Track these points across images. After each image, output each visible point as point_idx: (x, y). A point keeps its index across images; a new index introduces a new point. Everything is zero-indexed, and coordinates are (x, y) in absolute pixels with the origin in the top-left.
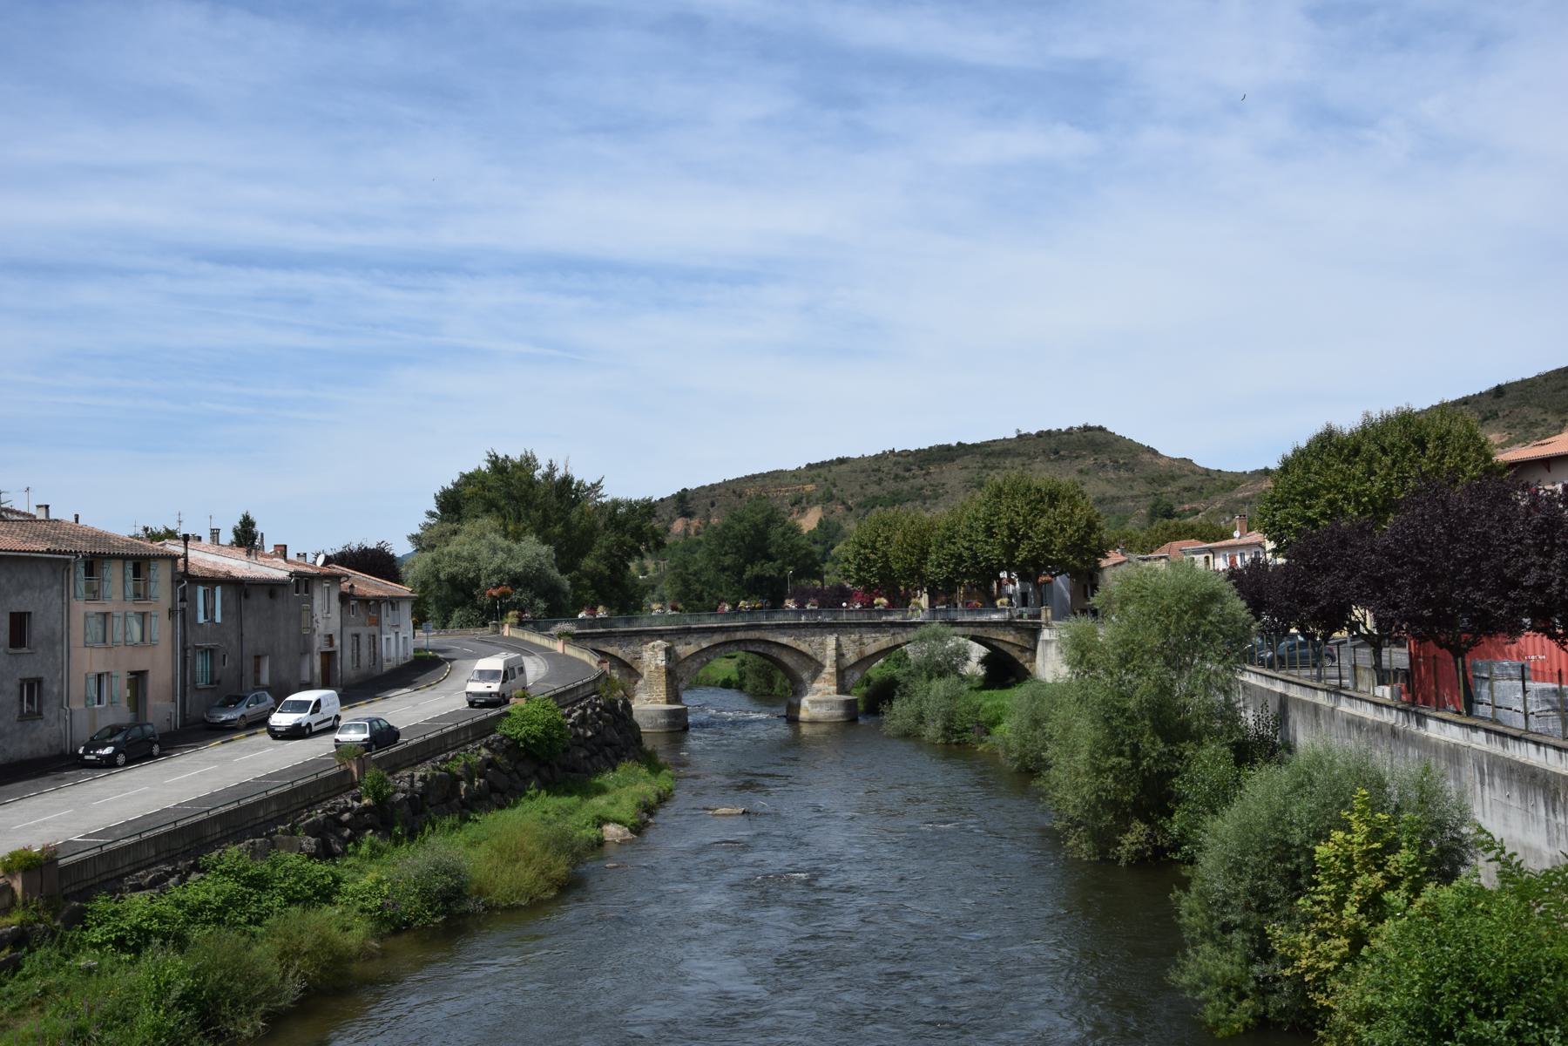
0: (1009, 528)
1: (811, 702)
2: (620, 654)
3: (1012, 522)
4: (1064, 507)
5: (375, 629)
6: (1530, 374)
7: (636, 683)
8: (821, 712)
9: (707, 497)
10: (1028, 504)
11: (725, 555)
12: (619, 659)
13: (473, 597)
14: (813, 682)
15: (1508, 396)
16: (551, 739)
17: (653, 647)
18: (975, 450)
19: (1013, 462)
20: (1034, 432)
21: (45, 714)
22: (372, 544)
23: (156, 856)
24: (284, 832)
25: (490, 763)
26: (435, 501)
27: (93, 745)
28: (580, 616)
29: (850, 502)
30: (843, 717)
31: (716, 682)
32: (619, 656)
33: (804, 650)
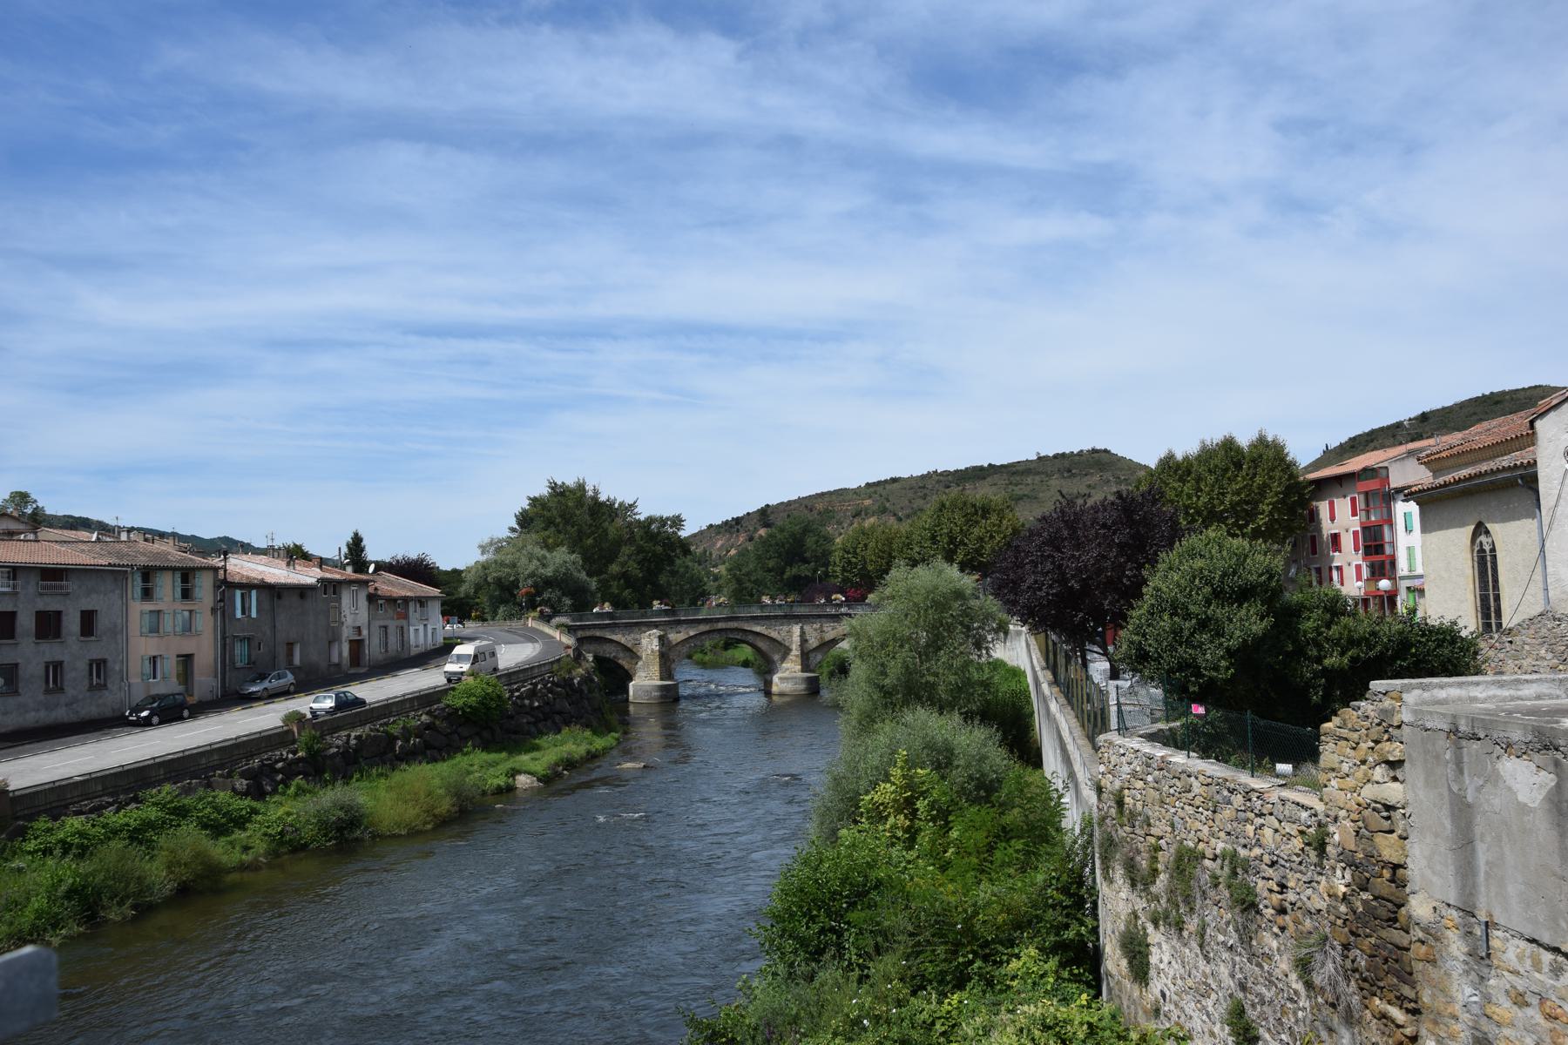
0: (949, 537)
1: (780, 679)
2: (623, 641)
4: (994, 518)
5: (404, 622)
6: (1449, 402)
9: (785, 511)
13: (515, 596)
14: (782, 663)
15: (1431, 421)
19: (1034, 480)
20: (1051, 455)
21: (109, 685)
22: (413, 556)
23: (103, 790)
24: (220, 776)
25: (428, 727)
27: (137, 709)
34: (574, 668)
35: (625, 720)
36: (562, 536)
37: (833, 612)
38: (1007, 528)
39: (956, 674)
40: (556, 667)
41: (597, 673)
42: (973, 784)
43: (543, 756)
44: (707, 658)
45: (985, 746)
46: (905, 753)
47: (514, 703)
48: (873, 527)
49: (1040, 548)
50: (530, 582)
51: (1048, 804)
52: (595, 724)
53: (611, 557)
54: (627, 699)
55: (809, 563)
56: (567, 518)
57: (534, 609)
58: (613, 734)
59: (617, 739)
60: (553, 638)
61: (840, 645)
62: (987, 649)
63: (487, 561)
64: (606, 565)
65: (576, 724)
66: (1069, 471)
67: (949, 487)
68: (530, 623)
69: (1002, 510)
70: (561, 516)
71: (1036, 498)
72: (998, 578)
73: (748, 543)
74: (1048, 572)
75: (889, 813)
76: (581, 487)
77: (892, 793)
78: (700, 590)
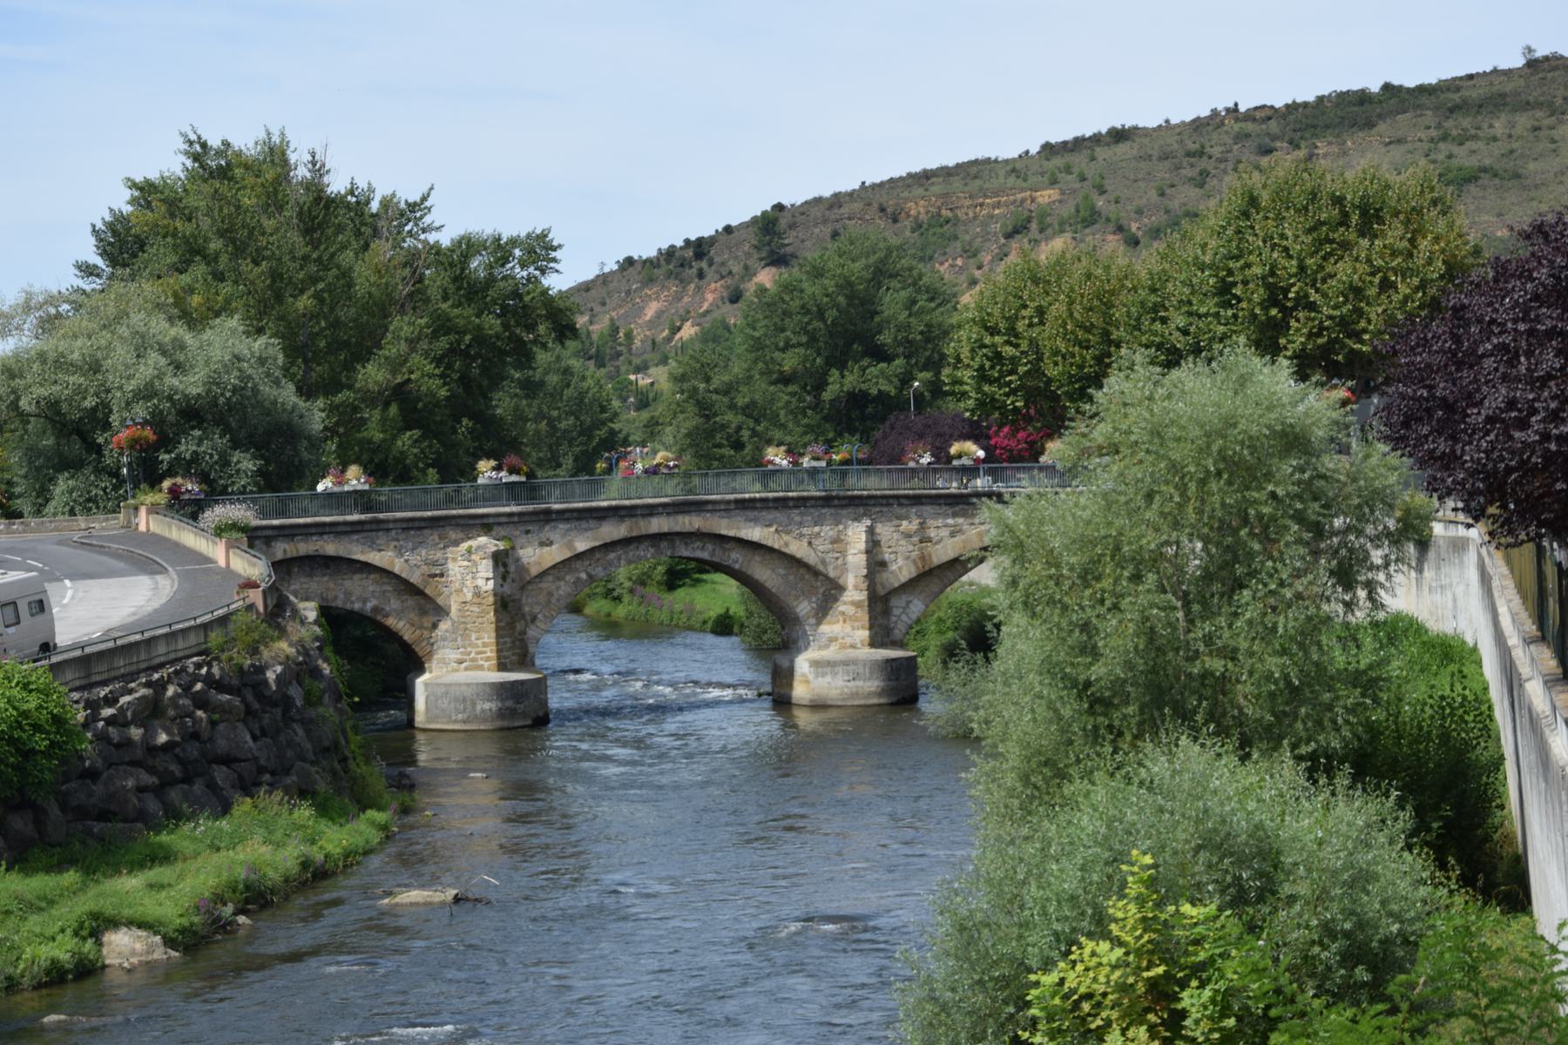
1: (816, 664)
2: (398, 566)
3: (1272, 273)
4: (1394, 234)
7: (435, 626)
8: (833, 686)
9: (825, 221)
10: (1309, 231)
11: (783, 350)
12: (397, 577)
13: (98, 449)
14: (819, 623)
17: (469, 551)
18: (1424, 100)
26: (93, 241)
28: (320, 487)
29: (1134, 227)
30: (880, 695)
31: (705, 622)
32: (397, 570)
33: (799, 555)
34: (265, 640)
35: (403, 775)
36: (226, 289)
37: (954, 487)
38: (1430, 262)
39: (1284, 652)
40: (215, 637)
41: (328, 651)
42: (1334, 947)
43: (181, 877)
44: (620, 612)
45: (1368, 846)
46: (1148, 860)
47: (102, 737)
48: (1060, 265)
49: (1526, 312)
50: (141, 411)
51: (1552, 1012)
52: (322, 787)
53: (363, 346)
54: (410, 723)
55: (889, 359)
56: (240, 240)
57: (154, 481)
58: (372, 814)
59: (384, 828)
60: (208, 560)
61: (972, 575)
62: (1371, 586)
63: (16, 355)
64: (349, 366)
65: (272, 786)
67: (1268, 151)
68: (144, 521)
69: (1418, 211)
70: (221, 234)
71: (1517, 176)
72: (1403, 396)
73: (728, 307)
74: (1549, 377)
75: (1108, 1023)
76: (276, 155)
77: (1114, 967)
78: (602, 433)
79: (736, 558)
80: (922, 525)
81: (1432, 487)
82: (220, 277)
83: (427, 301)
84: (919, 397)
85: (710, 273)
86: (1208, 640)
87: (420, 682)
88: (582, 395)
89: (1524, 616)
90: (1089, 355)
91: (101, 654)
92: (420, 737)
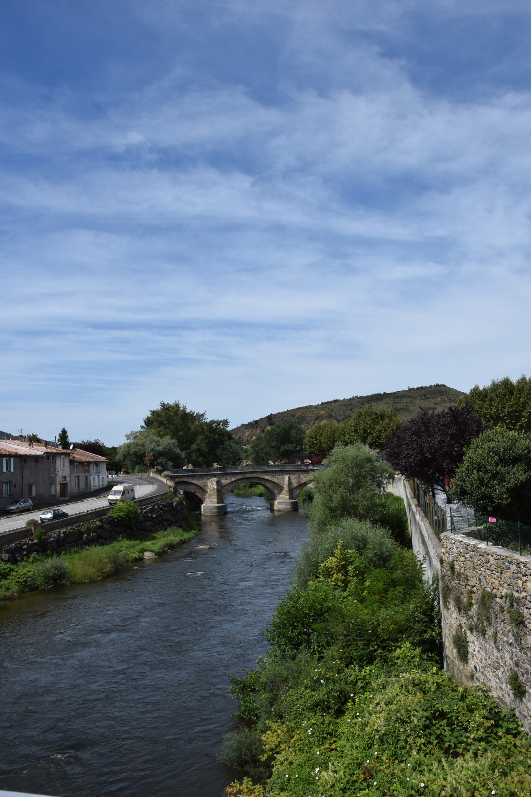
1: (278, 503)
2: (198, 483)
4: (387, 420)
5: (87, 474)
8: (282, 507)
13: (143, 461)
14: (279, 494)
16: (130, 518)
22: (92, 440)
25: (99, 527)
28: (184, 468)
34: (173, 497)
36: (167, 430)
37: (305, 468)
39: (368, 500)
40: (164, 497)
43: (158, 542)
46: (342, 542)
47: (143, 515)
48: (325, 426)
49: (410, 436)
50: (151, 454)
54: (200, 513)
57: (153, 467)
58: (193, 531)
59: (195, 534)
60: (163, 482)
62: (384, 488)
63: (129, 443)
65: (175, 526)
66: (425, 396)
67: (363, 404)
68: (151, 474)
69: (391, 416)
70: (167, 420)
71: (408, 410)
72: (389, 452)
73: (261, 433)
74: (415, 449)
75: (334, 573)
76: (177, 405)
79: (263, 482)
80: (299, 476)
81: (395, 469)
82: (166, 428)
83: (204, 432)
84: (298, 450)
85: (258, 427)
86: (353, 498)
87: (202, 506)
88: (234, 450)
89: (411, 493)
90: (331, 443)
91: (143, 500)
92: (203, 517)
